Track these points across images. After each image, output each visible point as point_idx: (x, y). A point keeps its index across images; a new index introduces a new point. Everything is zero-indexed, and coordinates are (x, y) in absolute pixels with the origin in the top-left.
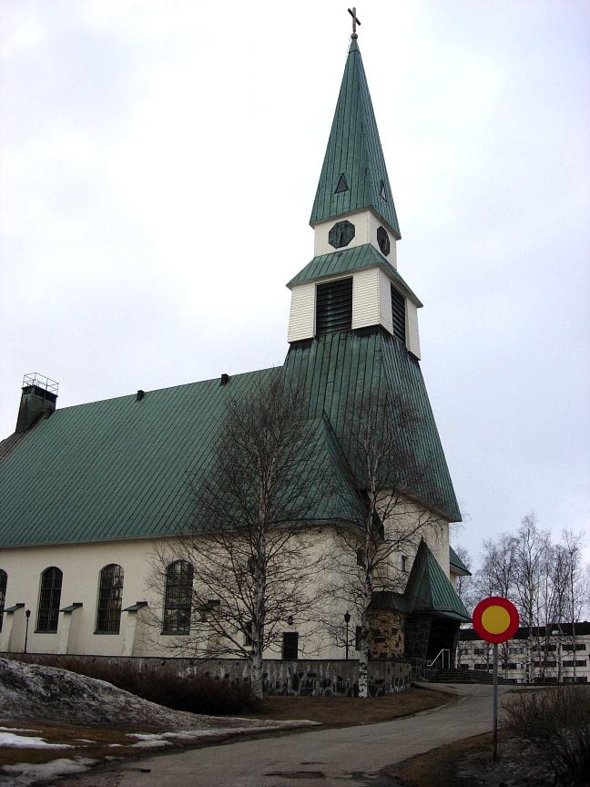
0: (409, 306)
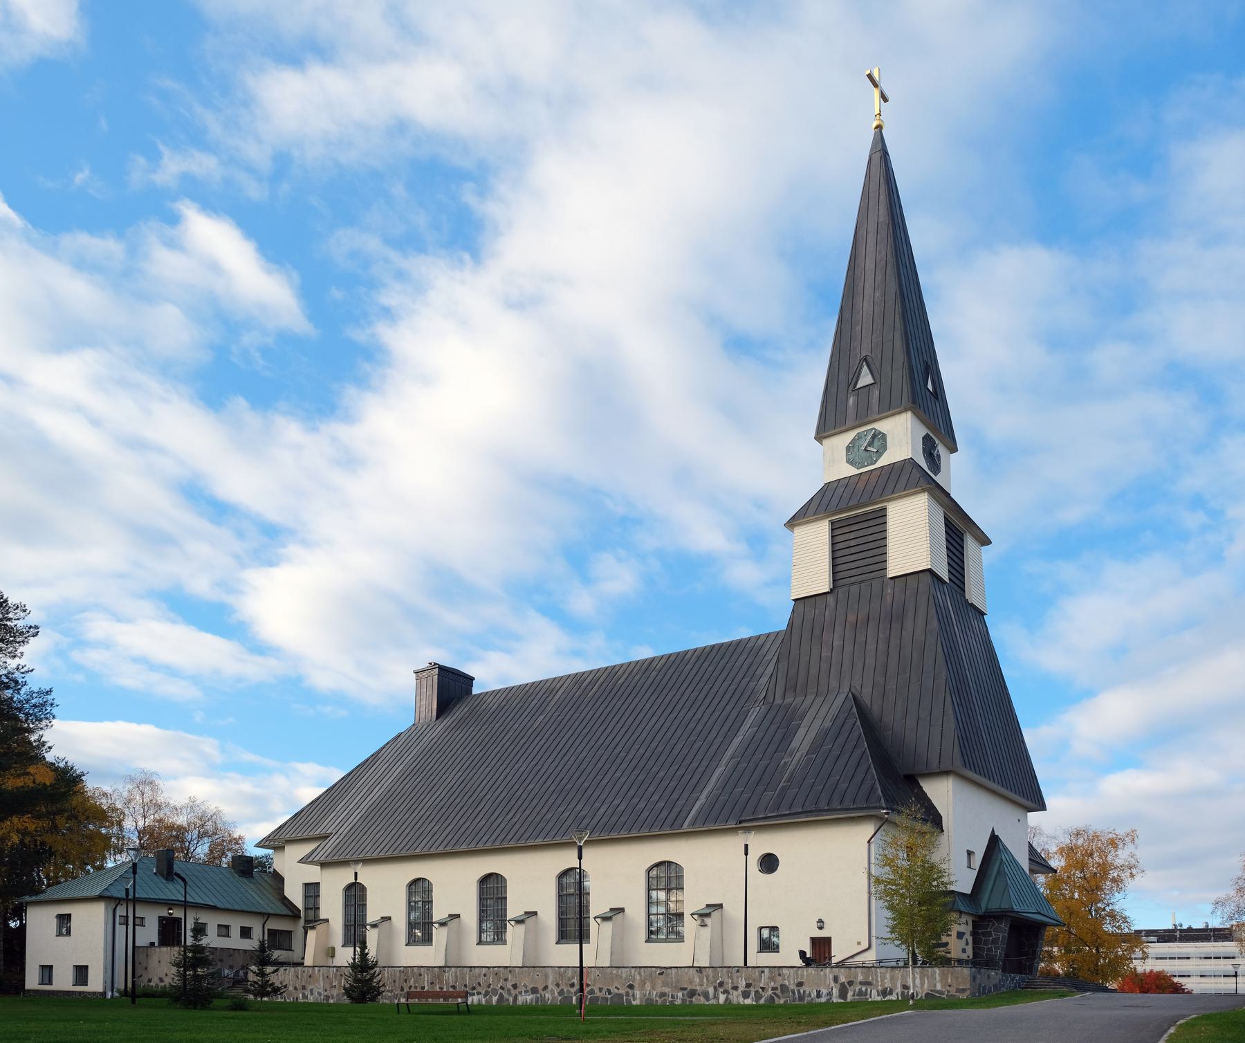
0: (970, 543)
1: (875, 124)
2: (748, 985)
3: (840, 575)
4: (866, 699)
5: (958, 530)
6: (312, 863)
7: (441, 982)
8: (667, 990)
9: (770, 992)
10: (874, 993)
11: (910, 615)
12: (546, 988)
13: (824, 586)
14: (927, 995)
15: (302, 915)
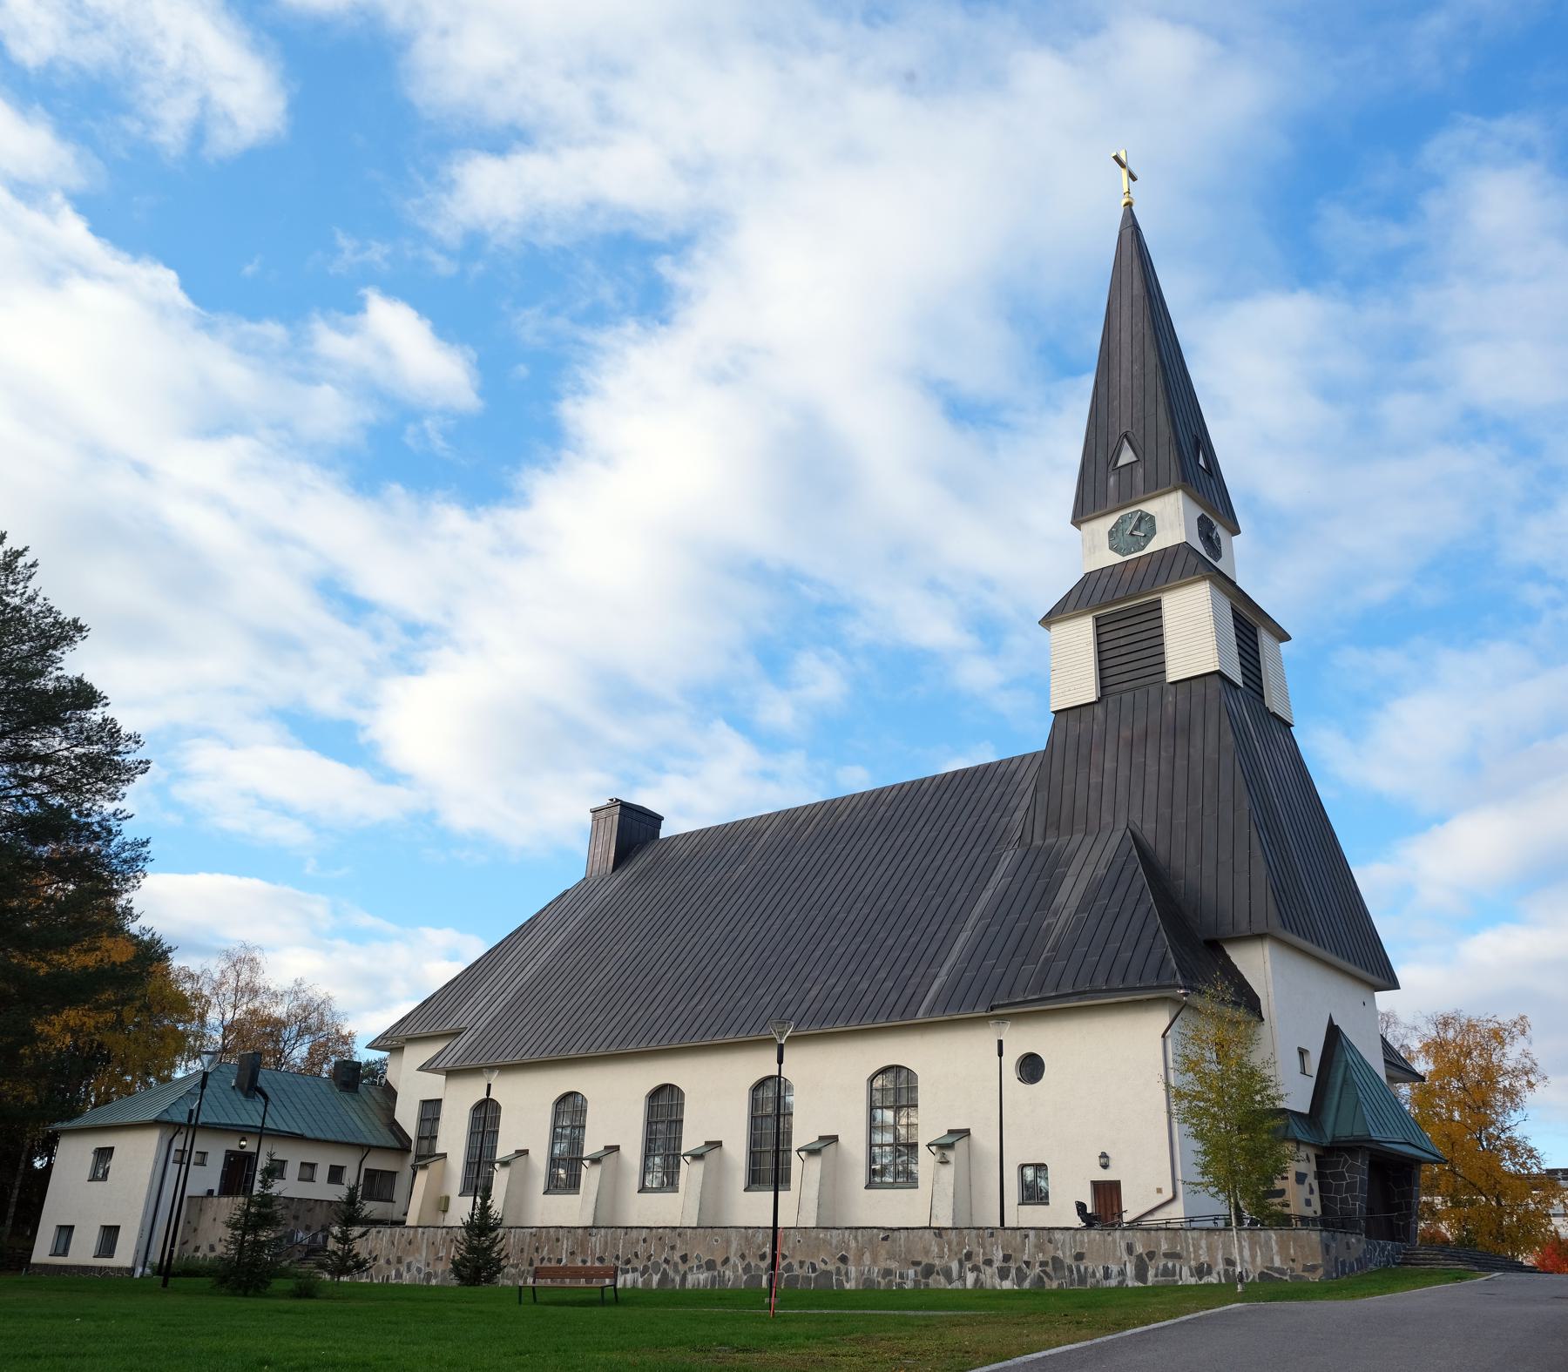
0: (1265, 640)
1: (1124, 201)
2: (1007, 1258)
6: (435, 1071)
8: (893, 1265)
9: (1038, 1270)
10: (1185, 1270)
12: (726, 1260)
13: (1090, 695)
14: (1262, 1274)
15: (413, 1147)
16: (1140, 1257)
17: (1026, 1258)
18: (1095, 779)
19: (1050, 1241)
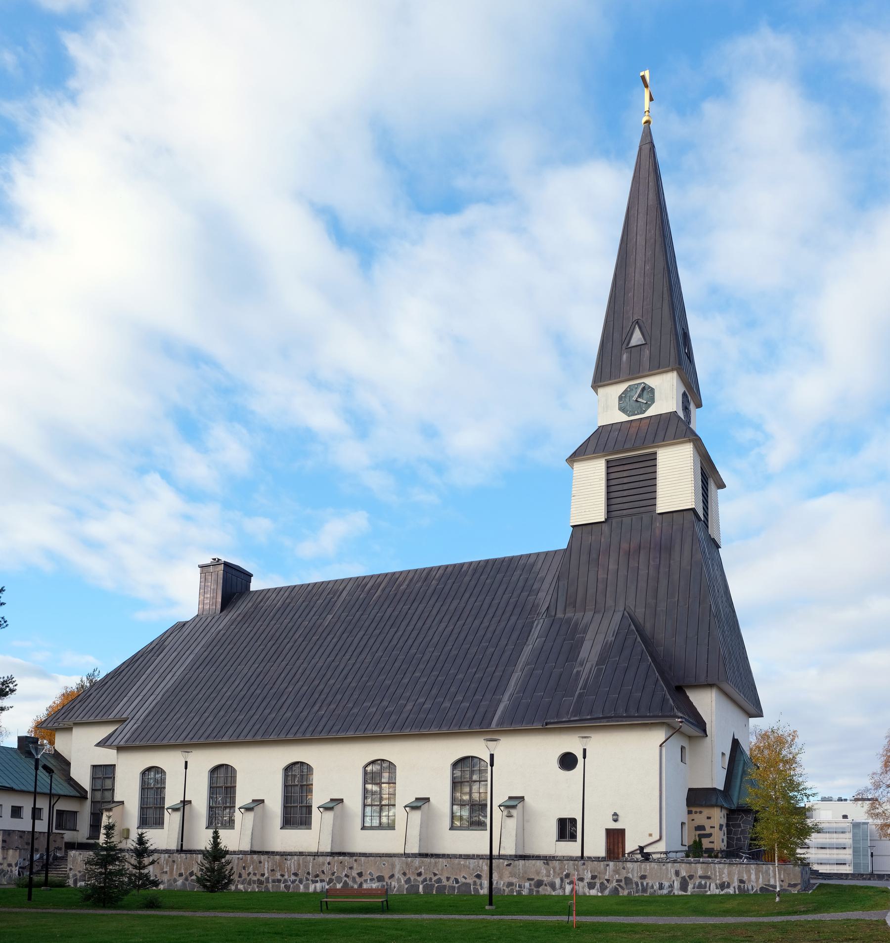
0: (712, 486)
1: (645, 119)
2: (594, 877)
3: (613, 508)
4: (640, 618)
5: (708, 476)
6: (110, 747)
7: (282, 869)
8: (514, 880)
9: (615, 884)
10: (713, 886)
11: (677, 548)
12: (392, 876)
13: (600, 516)
14: (761, 889)
15: (89, 796)
16: (683, 878)
17: (607, 877)
18: (602, 575)
19: (624, 868)
